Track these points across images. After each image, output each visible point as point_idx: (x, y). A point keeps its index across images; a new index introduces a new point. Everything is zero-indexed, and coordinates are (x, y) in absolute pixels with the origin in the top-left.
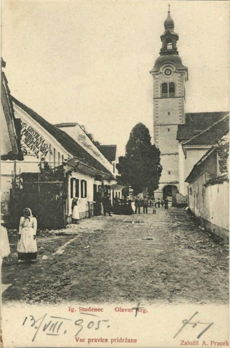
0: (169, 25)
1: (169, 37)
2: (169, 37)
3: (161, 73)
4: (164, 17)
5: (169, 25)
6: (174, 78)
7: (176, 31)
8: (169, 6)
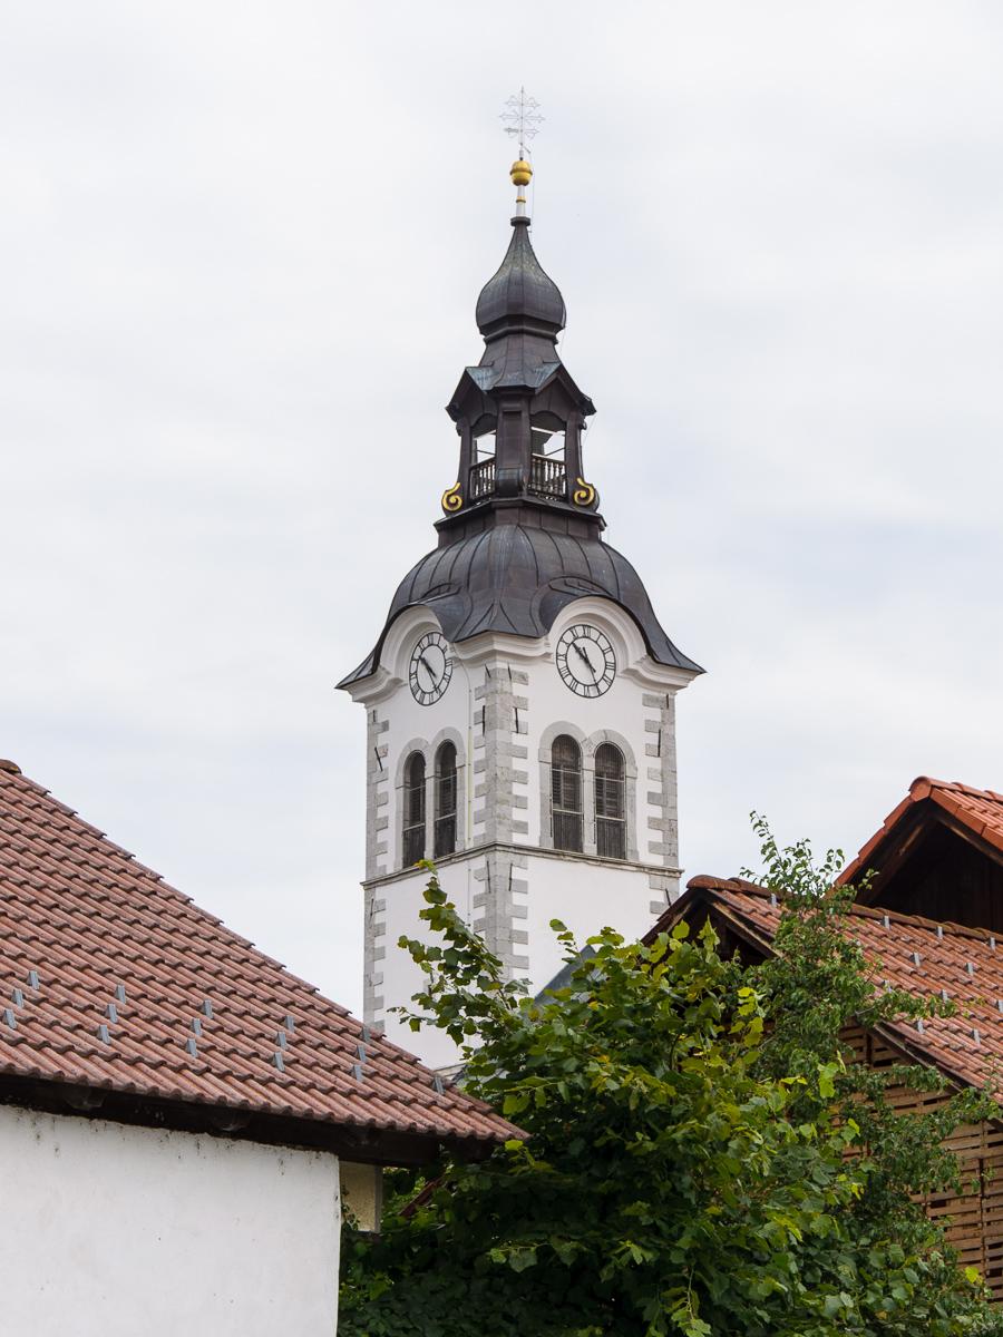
0: (520, 312)
1: (519, 392)
2: (519, 392)
3: (397, 682)
4: (486, 261)
5: (520, 312)
6: (614, 714)
7: (578, 351)
8: (521, 182)
